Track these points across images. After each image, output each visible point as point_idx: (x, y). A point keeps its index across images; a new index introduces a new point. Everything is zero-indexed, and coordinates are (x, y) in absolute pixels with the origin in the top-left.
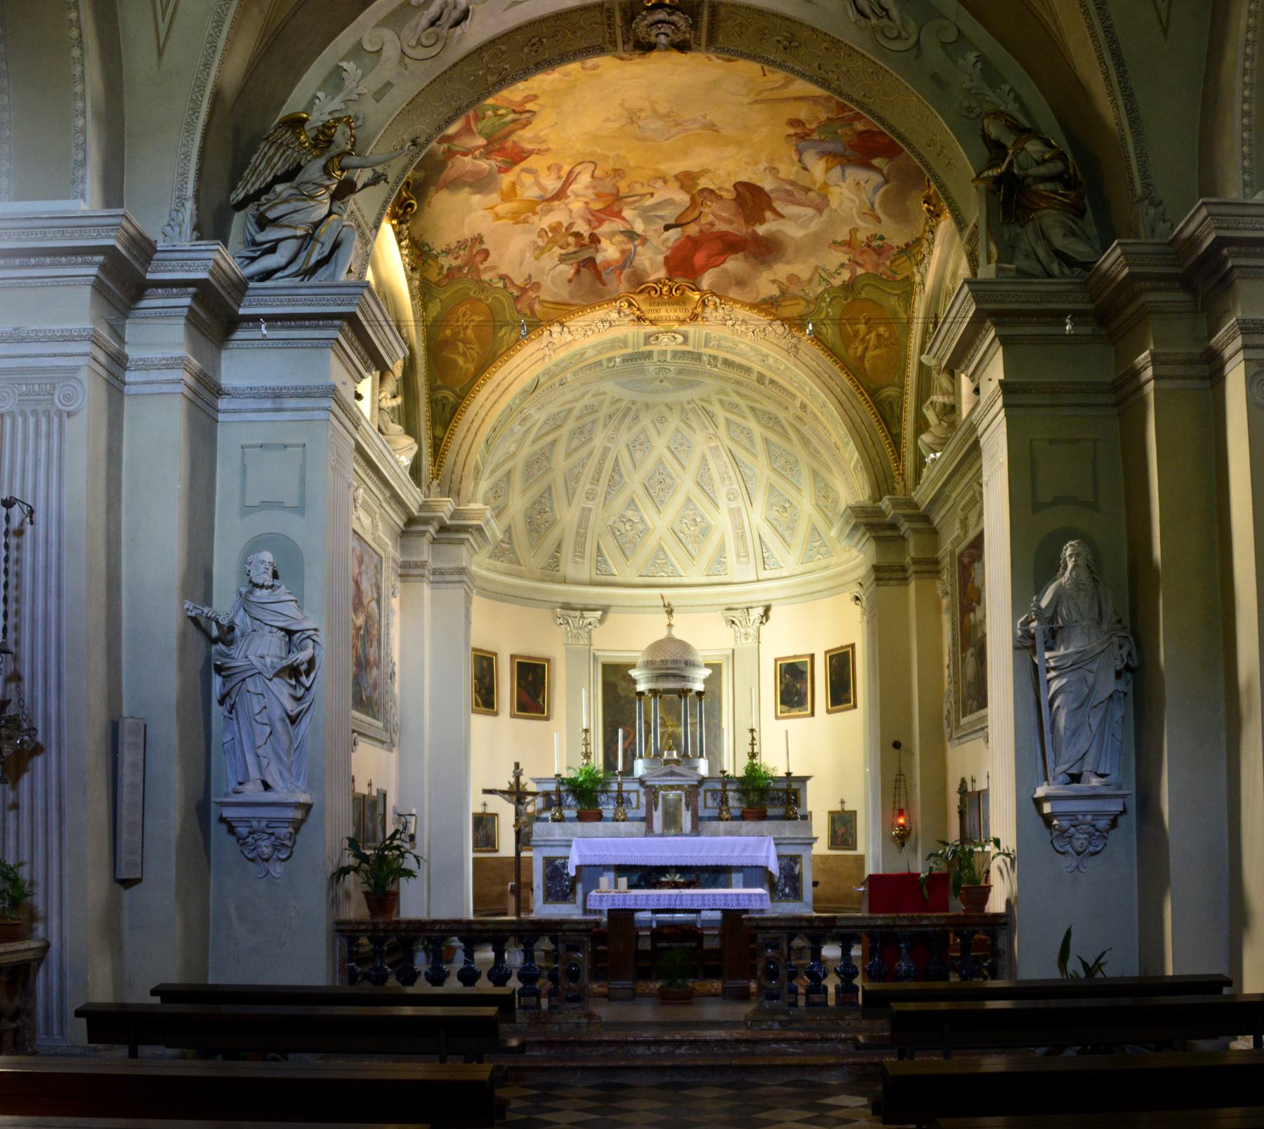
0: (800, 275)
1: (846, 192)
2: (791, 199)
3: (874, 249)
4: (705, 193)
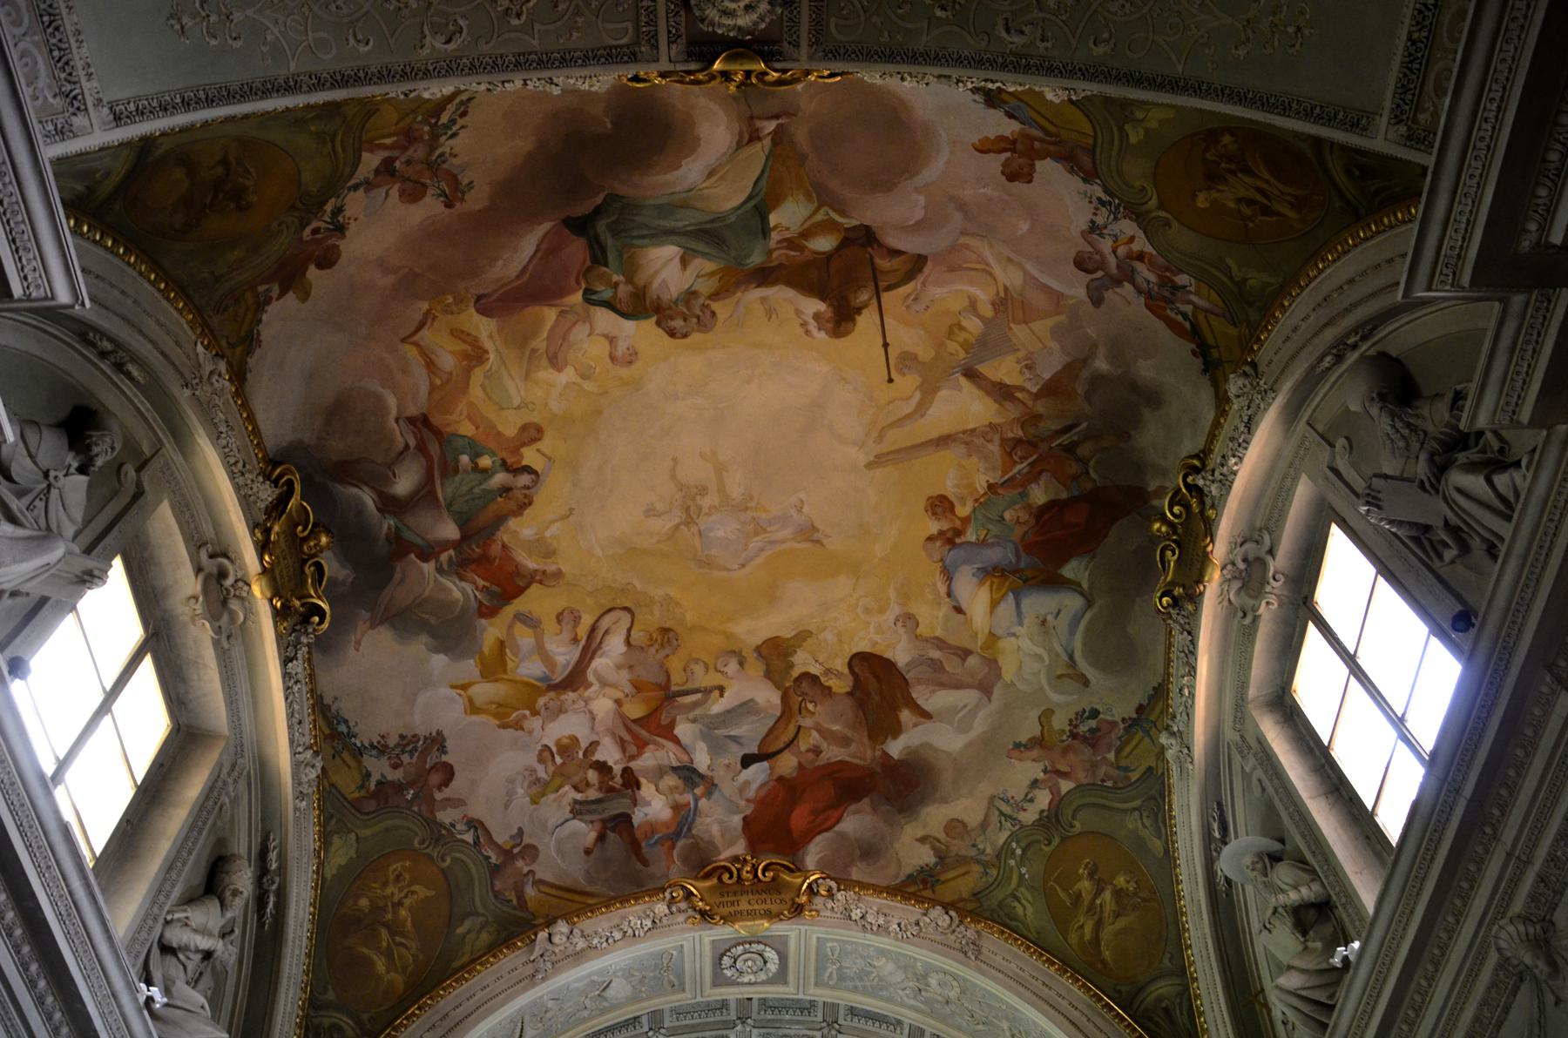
0: (966, 819)
1: (1026, 644)
2: (940, 678)
3: (1085, 739)
4: (804, 685)
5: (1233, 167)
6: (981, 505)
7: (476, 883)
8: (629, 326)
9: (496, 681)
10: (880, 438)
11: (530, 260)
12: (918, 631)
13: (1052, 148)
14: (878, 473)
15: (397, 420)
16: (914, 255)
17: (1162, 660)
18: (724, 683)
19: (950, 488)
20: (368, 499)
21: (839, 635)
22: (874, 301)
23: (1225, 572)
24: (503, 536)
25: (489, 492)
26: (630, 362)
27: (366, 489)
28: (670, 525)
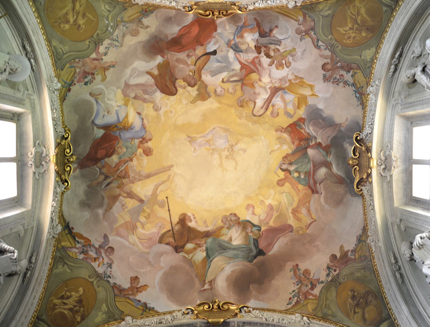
0: (131, 37)
1: (113, 103)
2: (143, 87)
3: (88, 74)
4: (193, 82)
5: (75, 309)
6: (134, 153)
7: (320, 26)
8: (248, 218)
9: (302, 95)
10: (169, 176)
11: (275, 243)
12: (153, 105)
13: (126, 293)
14: (169, 164)
15: (321, 193)
16: (162, 243)
17: (64, 111)
18: (222, 84)
19: (145, 159)
20: (335, 169)
21: (181, 102)
22: (173, 226)
23: (49, 159)
24: (293, 147)
25: (296, 164)
26: (248, 205)
27: (335, 173)
28: (238, 145)
